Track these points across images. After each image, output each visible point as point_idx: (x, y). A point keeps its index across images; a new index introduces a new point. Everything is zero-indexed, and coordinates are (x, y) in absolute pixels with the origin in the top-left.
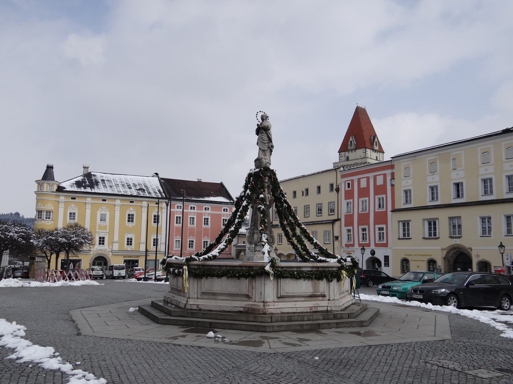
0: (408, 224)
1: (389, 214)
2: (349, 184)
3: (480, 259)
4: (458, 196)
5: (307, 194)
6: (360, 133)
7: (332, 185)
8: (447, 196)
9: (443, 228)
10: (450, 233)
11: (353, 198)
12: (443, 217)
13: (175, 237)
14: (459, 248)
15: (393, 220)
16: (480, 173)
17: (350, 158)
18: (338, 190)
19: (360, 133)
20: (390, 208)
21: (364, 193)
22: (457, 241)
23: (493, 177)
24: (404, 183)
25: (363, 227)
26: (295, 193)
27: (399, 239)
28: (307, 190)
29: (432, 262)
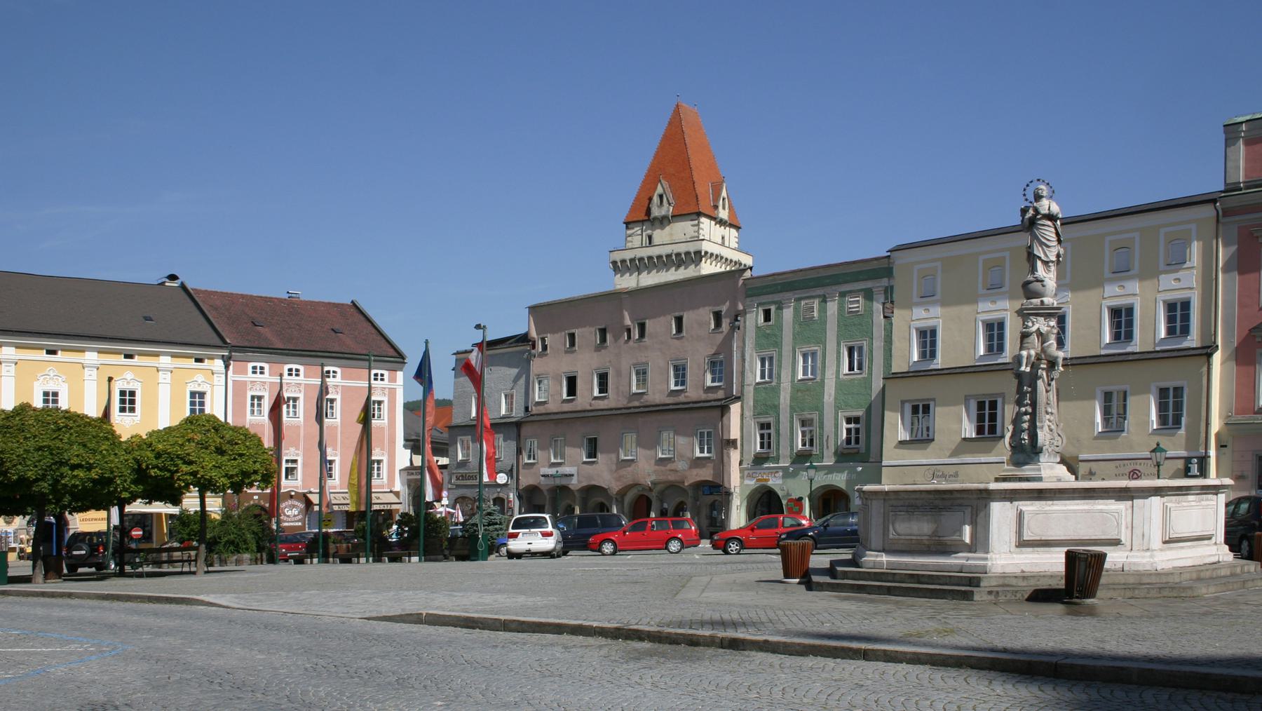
11: (778, 344)
17: (656, 240)
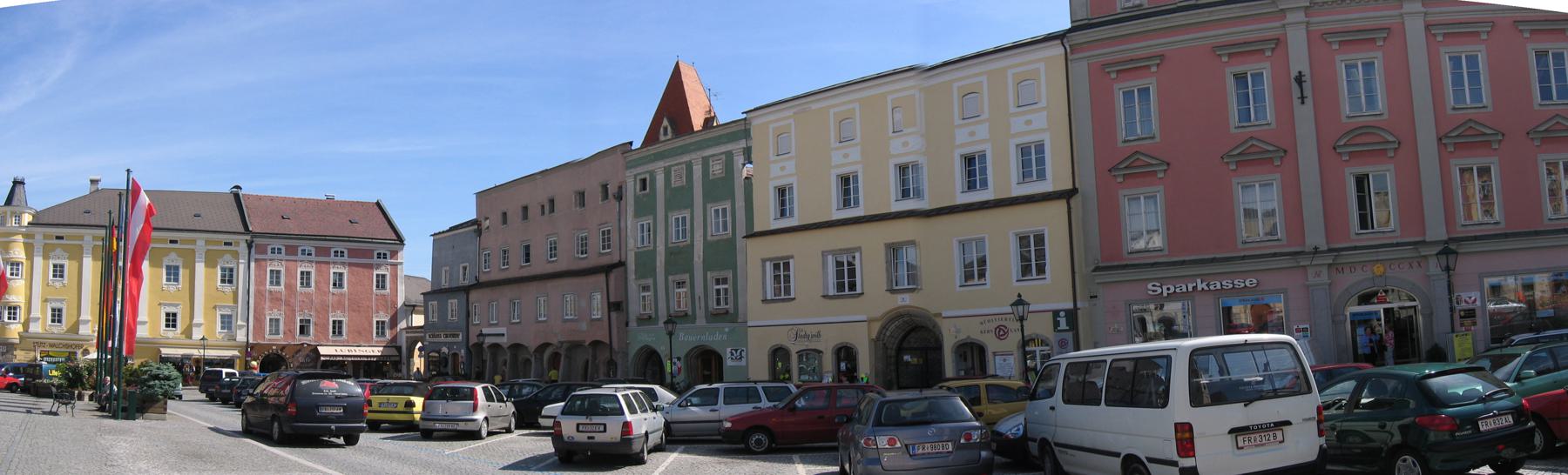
0: (787, 266)
1: (740, 242)
2: (644, 181)
3: (962, 337)
4: (846, 203)
5: (552, 210)
6: (673, 103)
7: (605, 187)
8: (880, 194)
9: (871, 273)
10: (889, 280)
12: (870, 244)
13: (267, 312)
14: (900, 316)
15: (754, 255)
16: (958, 142)
18: (619, 197)
19: (673, 103)
20: (741, 230)
21: (679, 198)
22: (904, 300)
23: (988, 149)
24: (775, 170)
25: (679, 278)
26: (525, 209)
27: (765, 301)
28: (552, 201)
29: (846, 353)
